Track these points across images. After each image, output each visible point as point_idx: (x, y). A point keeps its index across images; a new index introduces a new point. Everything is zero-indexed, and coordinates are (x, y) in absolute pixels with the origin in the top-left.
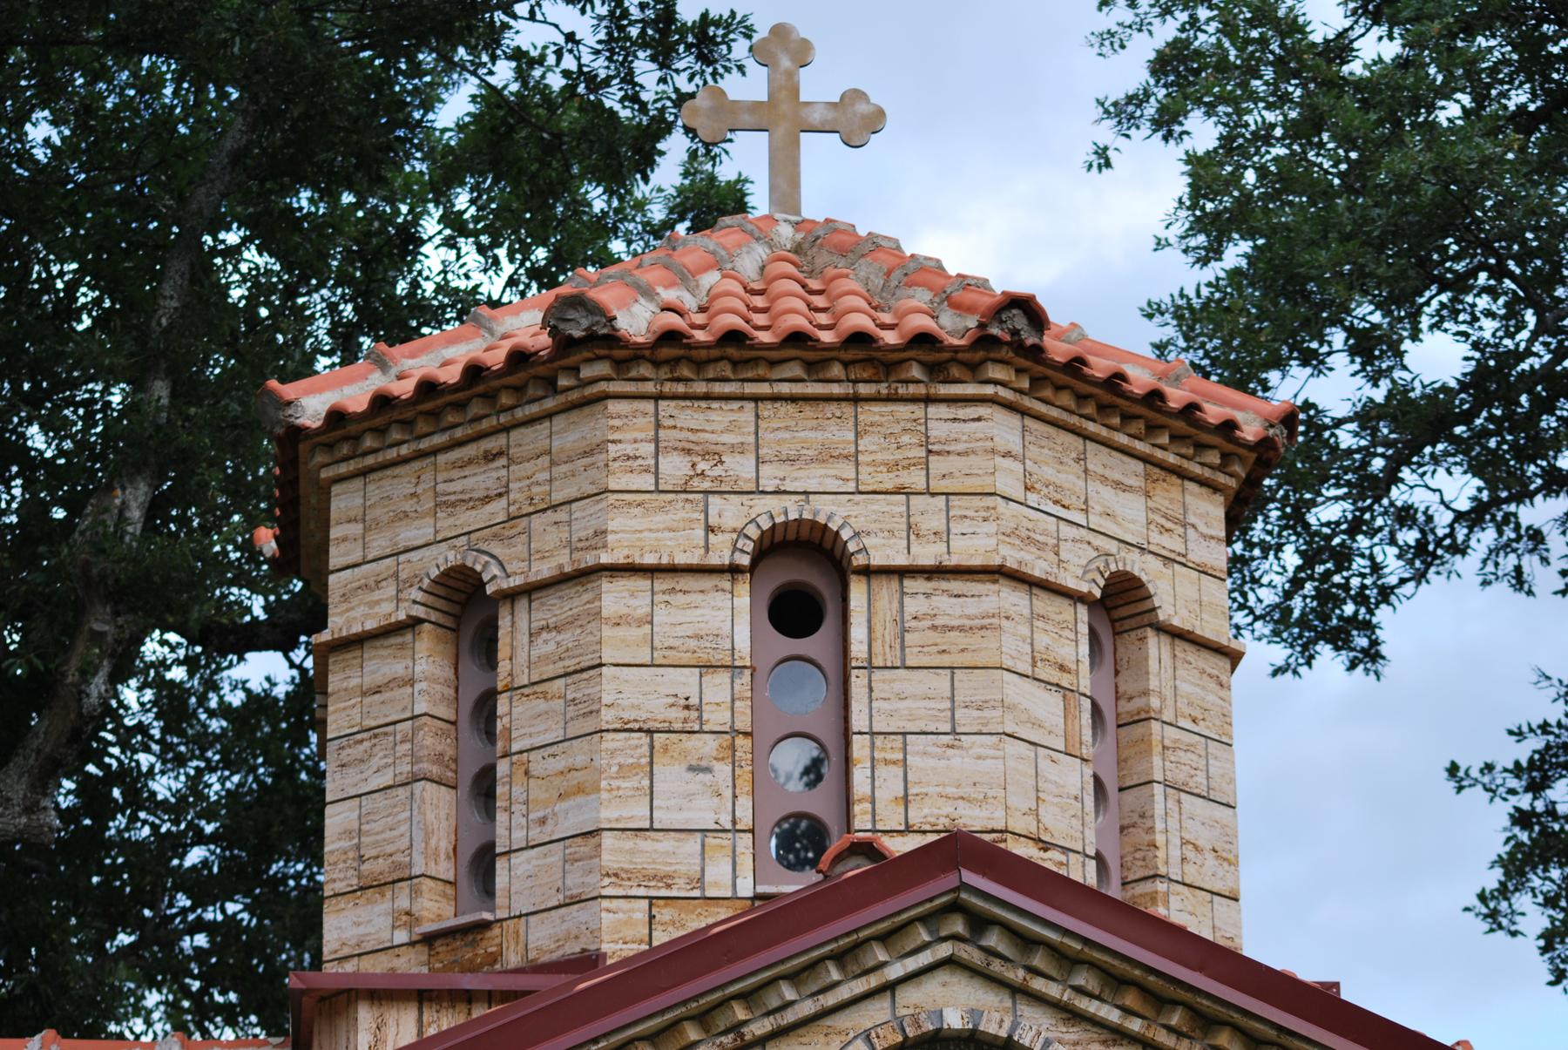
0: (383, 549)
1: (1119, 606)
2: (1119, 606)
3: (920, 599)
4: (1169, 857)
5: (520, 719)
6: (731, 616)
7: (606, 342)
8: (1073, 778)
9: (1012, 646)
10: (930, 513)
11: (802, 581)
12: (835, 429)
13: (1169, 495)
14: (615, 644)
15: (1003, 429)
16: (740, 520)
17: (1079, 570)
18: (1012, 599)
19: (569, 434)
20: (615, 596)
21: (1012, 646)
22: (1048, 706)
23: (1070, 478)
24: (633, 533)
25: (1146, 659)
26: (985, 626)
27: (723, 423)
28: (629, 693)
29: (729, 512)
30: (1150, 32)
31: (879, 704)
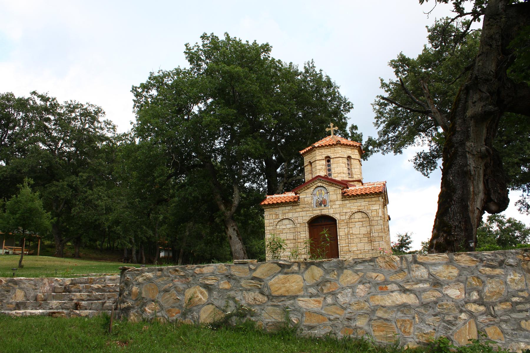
0: (307, 160)
1: (349, 158)
2: (349, 158)
3: (335, 159)
4: (354, 172)
5: (314, 170)
6: (324, 162)
7: (315, 147)
8: (346, 169)
9: (341, 162)
10: (335, 154)
11: (328, 159)
12: (329, 150)
13: (353, 150)
14: (317, 165)
15: (340, 148)
16: (324, 156)
17: (346, 156)
18: (341, 159)
19: (314, 153)
20: (317, 162)
21: (341, 162)
22: (344, 165)
23: (345, 151)
24: (318, 158)
25: (238, 235)
26: (339, 160)
27: (323, 151)
28: (318, 167)
29: (323, 156)
30: (197, 43)
31: (332, 166)
